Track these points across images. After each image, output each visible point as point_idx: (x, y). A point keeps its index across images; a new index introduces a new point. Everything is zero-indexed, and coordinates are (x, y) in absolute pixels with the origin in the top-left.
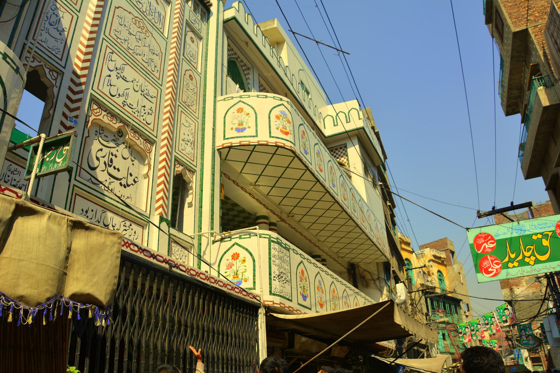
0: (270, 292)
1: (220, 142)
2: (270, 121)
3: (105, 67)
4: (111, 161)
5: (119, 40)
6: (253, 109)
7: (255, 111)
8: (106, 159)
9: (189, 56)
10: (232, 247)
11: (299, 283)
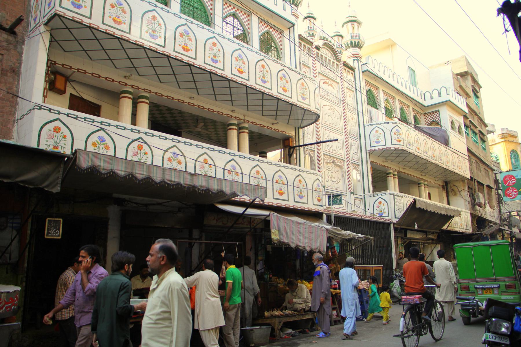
1: (369, 148)
4: (332, 175)
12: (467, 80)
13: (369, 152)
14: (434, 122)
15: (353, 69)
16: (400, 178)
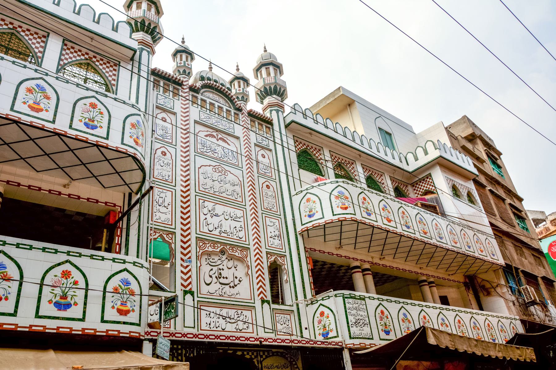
0: (350, 337)
1: (299, 228)
2: (331, 202)
3: (202, 214)
4: (220, 274)
5: (207, 191)
6: (317, 196)
7: (319, 198)
8: (216, 274)
9: (263, 170)
10: (319, 307)
11: (379, 322)
12: (477, 144)
13: (302, 234)
14: (427, 192)
15: (269, 122)
16: (375, 276)
